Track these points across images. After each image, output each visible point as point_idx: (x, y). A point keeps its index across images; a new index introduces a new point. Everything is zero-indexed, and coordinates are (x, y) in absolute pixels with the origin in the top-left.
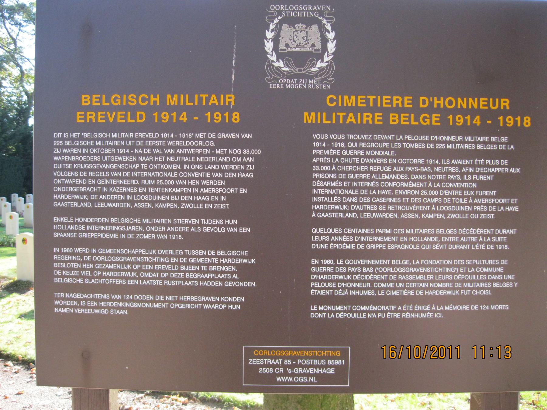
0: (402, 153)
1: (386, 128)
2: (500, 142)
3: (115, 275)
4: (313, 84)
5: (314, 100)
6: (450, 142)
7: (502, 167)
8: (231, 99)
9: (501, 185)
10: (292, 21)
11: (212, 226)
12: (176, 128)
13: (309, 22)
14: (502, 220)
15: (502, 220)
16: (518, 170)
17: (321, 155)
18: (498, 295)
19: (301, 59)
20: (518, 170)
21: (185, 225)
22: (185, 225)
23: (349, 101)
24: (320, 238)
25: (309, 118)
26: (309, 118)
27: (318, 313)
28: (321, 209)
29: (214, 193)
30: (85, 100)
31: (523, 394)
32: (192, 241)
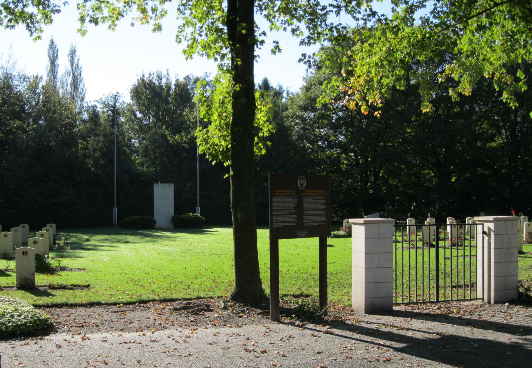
0: (314, 199)
1: (311, 196)
2: (324, 197)
3: (280, 220)
4: (304, 189)
5: (303, 191)
6: (319, 198)
7: (324, 201)
8: (294, 191)
9: (324, 204)
10: (301, 179)
11: (292, 211)
12: (288, 196)
13: (303, 179)
14: (325, 209)
15: (325, 209)
16: (225, 177)
17: (304, 200)
18: (325, 221)
19: (302, 185)
20: (225, 177)
21: (289, 211)
22: (289, 211)
23: (308, 191)
24: (306, 213)
25: (303, 194)
26: (303, 194)
27: (305, 225)
28: (305, 208)
29: (292, 206)
30: (277, 191)
31: (280, 241)
32: (290, 214)
